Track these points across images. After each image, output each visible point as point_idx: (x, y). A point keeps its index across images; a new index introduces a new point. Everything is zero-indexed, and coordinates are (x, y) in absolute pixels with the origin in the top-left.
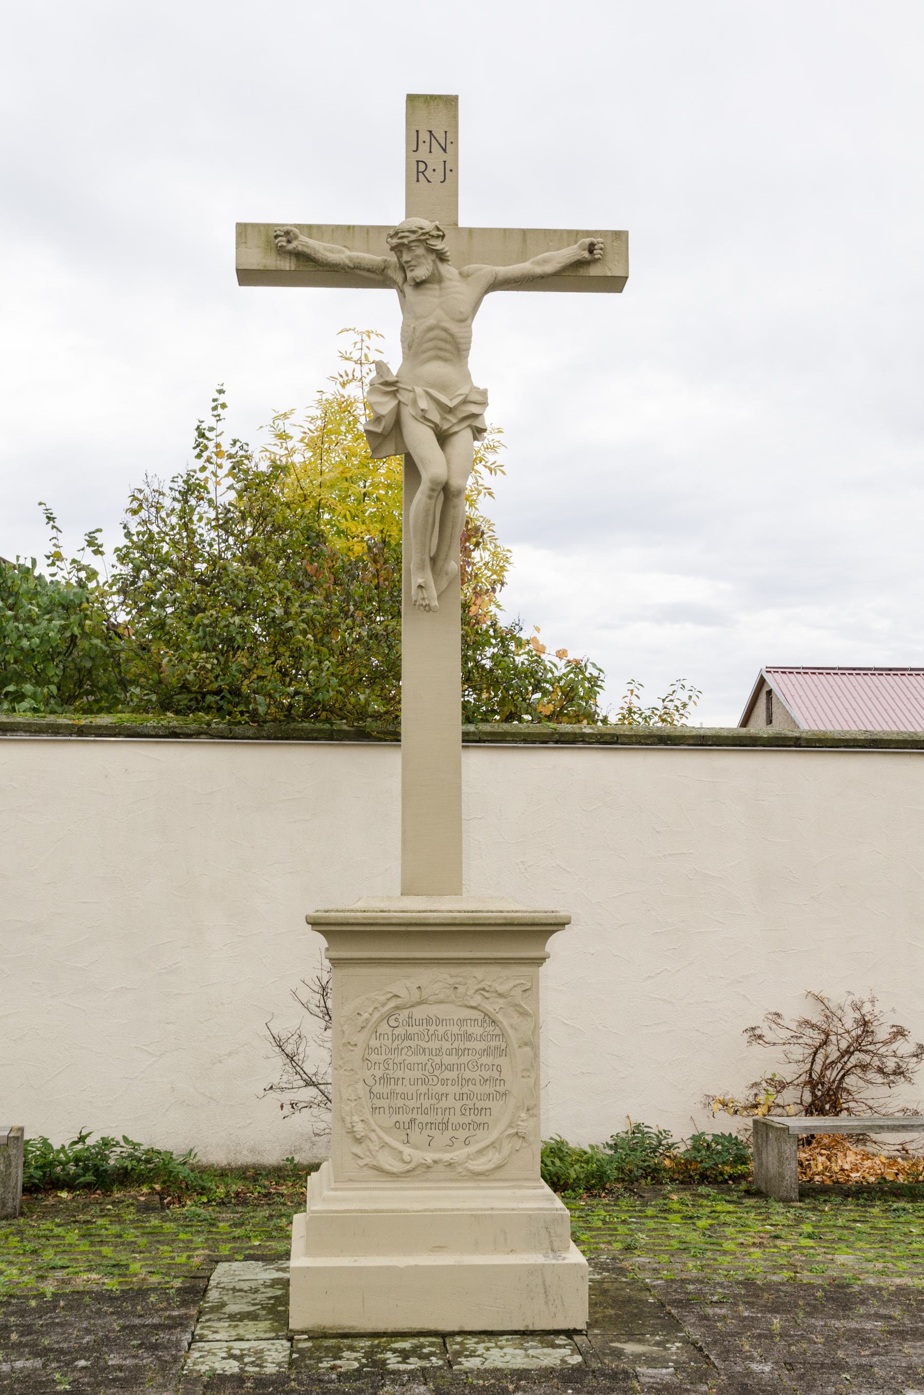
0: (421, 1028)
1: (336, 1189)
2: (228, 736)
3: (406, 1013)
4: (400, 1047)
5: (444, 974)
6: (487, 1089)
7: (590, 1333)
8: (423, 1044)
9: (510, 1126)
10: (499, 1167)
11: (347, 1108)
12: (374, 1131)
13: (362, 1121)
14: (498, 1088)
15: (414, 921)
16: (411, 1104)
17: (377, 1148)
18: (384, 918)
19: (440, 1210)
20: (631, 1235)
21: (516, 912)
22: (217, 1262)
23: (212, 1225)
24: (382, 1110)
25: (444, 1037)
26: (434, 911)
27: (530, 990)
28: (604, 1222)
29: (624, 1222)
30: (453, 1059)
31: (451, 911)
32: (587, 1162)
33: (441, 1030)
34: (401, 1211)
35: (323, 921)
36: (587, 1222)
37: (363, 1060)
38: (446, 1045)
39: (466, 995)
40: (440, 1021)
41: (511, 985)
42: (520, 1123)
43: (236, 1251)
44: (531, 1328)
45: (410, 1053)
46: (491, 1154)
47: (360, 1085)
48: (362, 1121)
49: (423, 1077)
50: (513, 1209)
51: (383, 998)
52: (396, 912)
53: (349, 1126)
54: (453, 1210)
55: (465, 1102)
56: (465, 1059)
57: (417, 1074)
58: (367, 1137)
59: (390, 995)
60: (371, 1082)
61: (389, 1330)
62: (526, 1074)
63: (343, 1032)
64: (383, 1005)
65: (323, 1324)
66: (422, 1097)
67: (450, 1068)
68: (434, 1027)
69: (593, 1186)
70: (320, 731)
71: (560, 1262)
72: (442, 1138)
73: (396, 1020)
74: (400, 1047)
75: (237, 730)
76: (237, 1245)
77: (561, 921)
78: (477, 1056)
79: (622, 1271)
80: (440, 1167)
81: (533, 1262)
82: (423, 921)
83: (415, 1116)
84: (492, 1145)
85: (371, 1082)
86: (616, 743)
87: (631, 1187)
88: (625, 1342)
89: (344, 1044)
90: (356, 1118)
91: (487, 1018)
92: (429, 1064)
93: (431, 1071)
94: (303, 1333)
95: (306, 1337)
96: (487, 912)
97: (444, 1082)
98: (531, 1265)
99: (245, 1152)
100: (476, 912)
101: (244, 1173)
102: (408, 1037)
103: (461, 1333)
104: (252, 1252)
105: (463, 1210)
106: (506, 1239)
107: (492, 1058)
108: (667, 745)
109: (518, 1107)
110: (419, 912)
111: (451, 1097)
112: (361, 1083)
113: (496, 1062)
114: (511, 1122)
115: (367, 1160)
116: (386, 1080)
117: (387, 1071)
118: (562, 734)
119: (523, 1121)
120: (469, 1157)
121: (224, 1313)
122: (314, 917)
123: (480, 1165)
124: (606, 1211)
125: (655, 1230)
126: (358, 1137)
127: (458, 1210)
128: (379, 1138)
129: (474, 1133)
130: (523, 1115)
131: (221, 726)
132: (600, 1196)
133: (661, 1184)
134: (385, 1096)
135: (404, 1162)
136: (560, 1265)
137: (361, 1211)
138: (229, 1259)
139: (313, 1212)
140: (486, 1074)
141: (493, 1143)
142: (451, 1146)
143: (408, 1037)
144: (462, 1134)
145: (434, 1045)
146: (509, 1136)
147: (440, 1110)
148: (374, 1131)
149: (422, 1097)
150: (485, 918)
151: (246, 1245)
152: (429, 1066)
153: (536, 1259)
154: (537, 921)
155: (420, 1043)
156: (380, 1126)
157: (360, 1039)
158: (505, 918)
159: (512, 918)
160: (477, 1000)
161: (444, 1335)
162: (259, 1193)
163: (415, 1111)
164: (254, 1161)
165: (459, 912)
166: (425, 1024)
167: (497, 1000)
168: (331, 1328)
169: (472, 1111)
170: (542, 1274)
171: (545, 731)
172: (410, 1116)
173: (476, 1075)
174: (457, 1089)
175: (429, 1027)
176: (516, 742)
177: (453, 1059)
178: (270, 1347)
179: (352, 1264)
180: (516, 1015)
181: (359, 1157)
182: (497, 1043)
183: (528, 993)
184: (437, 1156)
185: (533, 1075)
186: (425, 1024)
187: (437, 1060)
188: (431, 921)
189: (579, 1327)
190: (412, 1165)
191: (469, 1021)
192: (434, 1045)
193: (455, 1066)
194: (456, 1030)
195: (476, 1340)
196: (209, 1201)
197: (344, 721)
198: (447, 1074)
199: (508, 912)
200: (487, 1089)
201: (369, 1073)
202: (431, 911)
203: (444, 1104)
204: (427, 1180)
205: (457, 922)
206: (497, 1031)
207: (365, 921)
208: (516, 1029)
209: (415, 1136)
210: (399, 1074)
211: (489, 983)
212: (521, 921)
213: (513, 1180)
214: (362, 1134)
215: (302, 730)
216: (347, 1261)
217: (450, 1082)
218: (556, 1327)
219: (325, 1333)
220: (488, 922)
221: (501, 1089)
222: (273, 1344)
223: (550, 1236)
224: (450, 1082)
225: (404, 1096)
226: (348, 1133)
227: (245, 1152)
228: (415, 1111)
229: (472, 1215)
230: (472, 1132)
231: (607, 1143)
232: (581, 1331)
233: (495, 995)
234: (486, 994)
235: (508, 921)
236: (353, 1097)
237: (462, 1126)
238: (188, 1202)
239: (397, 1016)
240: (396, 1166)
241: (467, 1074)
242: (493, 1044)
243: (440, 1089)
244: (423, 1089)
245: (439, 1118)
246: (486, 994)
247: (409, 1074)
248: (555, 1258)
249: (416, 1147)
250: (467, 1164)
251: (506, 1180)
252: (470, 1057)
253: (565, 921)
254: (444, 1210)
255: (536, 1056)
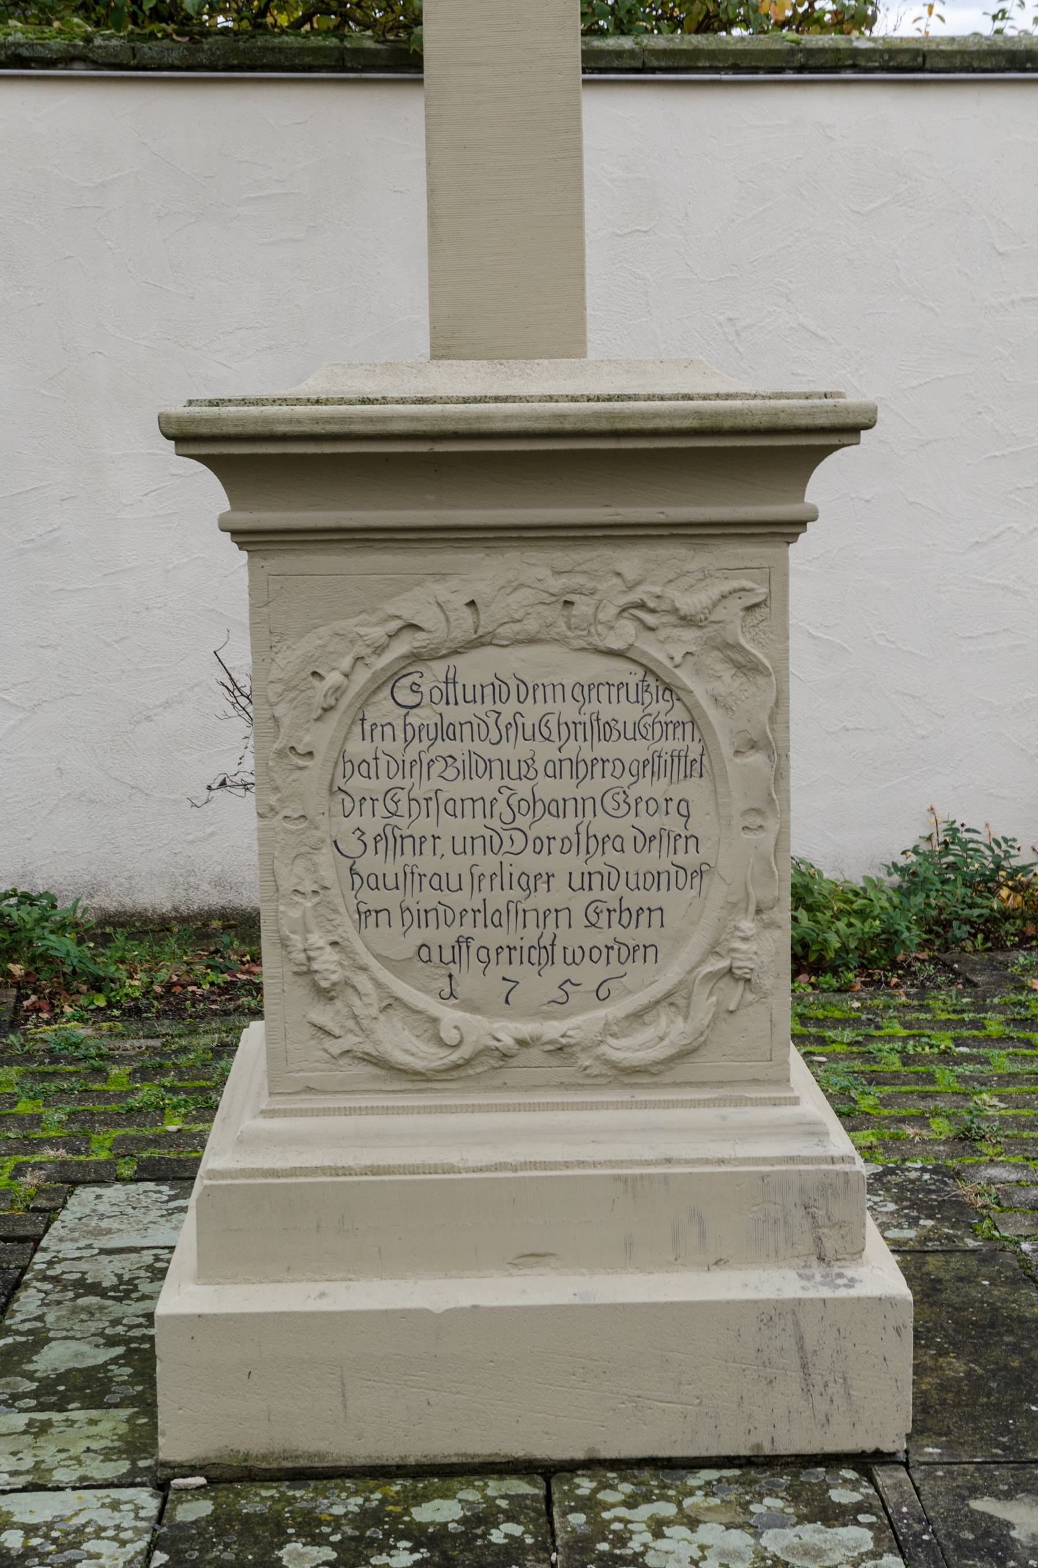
0: (479, 709)
1: (269, 1113)
2: (128, 66)
3: (439, 668)
4: (425, 759)
5: (538, 569)
6: (653, 860)
7: (914, 1458)
8: (485, 750)
9: (713, 951)
10: (684, 1054)
11: (295, 914)
12: (364, 969)
13: (334, 944)
14: (680, 858)
15: (451, 427)
16: (459, 900)
17: (374, 1011)
18: (371, 420)
19: (534, 1165)
20: (966, 1096)
21: (728, 396)
22: (76, 1183)
23: (99, 1073)
24: (383, 916)
25: (540, 731)
26: (505, 399)
27: (765, 607)
28: (907, 1059)
29: (945, 1056)
30: (563, 788)
31: (551, 398)
32: (863, 914)
33: (532, 712)
34: (434, 1169)
35: (204, 430)
36: (869, 1057)
37: (331, 793)
38: (545, 751)
39: (596, 621)
40: (527, 690)
41: (715, 592)
42: (738, 945)
43: (123, 1148)
44: (767, 1450)
45: (451, 773)
46: (663, 1020)
47: (326, 856)
48: (334, 944)
49: (487, 833)
50: (721, 1161)
51: (377, 633)
52: (402, 401)
53: (302, 957)
54: (567, 1165)
55: (596, 893)
56: (593, 787)
57: (472, 825)
58: (347, 983)
59: (394, 625)
60: (352, 847)
61: (412, 1461)
62: (755, 820)
63: (275, 719)
64: (379, 650)
65: (243, 1449)
66: (486, 883)
67: (555, 809)
68: (513, 705)
69: (873, 961)
70: (317, 51)
71: (842, 1293)
72: (538, 984)
73: (414, 688)
74: (425, 759)
75: (148, 50)
76: (132, 1131)
77: (850, 420)
78: (627, 779)
79: (959, 1212)
80: (535, 1054)
81: (773, 1296)
82: (476, 426)
83: (467, 930)
84: (667, 999)
85: (352, 847)
86: (921, 69)
87: (945, 956)
88: (1007, 1496)
89: (280, 754)
90: (317, 939)
91: (650, 680)
92: (502, 799)
93: (508, 817)
94: (192, 1470)
95: (201, 1481)
96: (650, 398)
97: (542, 845)
98: (766, 1302)
99: (205, 887)
100: (620, 398)
101: (205, 925)
102: (446, 731)
103: (592, 1465)
104: (156, 1153)
105: (595, 1164)
106: (703, 1235)
107: (664, 781)
108: (1024, 70)
109: (734, 905)
110: (466, 401)
111: (559, 883)
112: (328, 850)
113: (677, 792)
114: (717, 942)
115: (349, 1041)
116: (390, 840)
117: (395, 820)
118: (811, 52)
119: (745, 939)
120: (609, 1031)
121: (30, 1376)
122: (179, 420)
123: (634, 1048)
124: (907, 1025)
125: (1012, 1078)
126: (324, 984)
127: (581, 1164)
128: (378, 984)
129: (621, 970)
130: (747, 925)
131: (114, 42)
132: (888, 984)
133: (1003, 948)
134: (391, 883)
135: (441, 1043)
136: (843, 1301)
137: (335, 1171)
138: (102, 1177)
139: (213, 1174)
140: (650, 825)
141: (669, 995)
142: (561, 1002)
143: (446, 731)
144: (589, 974)
145: (513, 751)
146: (710, 977)
147: (531, 916)
148: (364, 969)
149: (486, 883)
150: (643, 415)
151: (148, 1132)
152: (501, 807)
153: (779, 1283)
154: (783, 421)
155: (478, 747)
156: (378, 957)
157: (320, 737)
158: (698, 414)
159: (716, 414)
160: (624, 634)
161: (549, 1471)
162: (212, 984)
163: (469, 918)
164: (222, 902)
165: (574, 399)
166: (489, 699)
167: (677, 632)
168: (264, 1458)
169: (615, 916)
170: (796, 1324)
171: (778, 47)
172: (456, 931)
173: (623, 826)
174: (575, 862)
175: (499, 707)
176: (717, 70)
177: (563, 788)
178: (105, 1518)
179: (311, 1306)
180: (727, 672)
181: (329, 1034)
182: (678, 745)
183: (759, 613)
184: (526, 1029)
185: (772, 825)
186: (489, 699)
187: (523, 788)
188: (498, 426)
189: (887, 1447)
190: (465, 1052)
191: (604, 690)
192: (513, 751)
193: (571, 804)
194: (569, 711)
195: (627, 1488)
196: (110, 1005)
197: (369, 33)
198: (549, 825)
199: (705, 397)
200: (653, 860)
201: (349, 824)
202: (497, 399)
203: (541, 899)
204: (505, 1087)
205: (568, 426)
206: (679, 714)
207: (318, 429)
208: (727, 708)
209: (470, 979)
210: (424, 826)
211: (657, 590)
212: (740, 422)
213: (720, 1084)
214: (334, 978)
215: (281, 50)
216: (321, 1247)
217: (555, 845)
218: (831, 1448)
219: (249, 1469)
220: (651, 425)
221: (690, 859)
222: (115, 1505)
223: (815, 1225)
224: (555, 845)
225: (440, 882)
226: (297, 974)
227: (205, 887)
228: (469, 918)
229: (617, 1178)
230: (615, 969)
231: (894, 865)
232: (893, 1454)
233: (672, 619)
234: (650, 619)
235: (707, 423)
236: (308, 886)
237: (590, 954)
238: (68, 1010)
239: (415, 678)
240: (424, 1055)
241: (602, 825)
242: (669, 746)
243: (531, 862)
244: (488, 863)
245: (531, 935)
246: (650, 619)
247: (449, 826)
248: (829, 1281)
249: (474, 1008)
250: (604, 1048)
251: (702, 1084)
252: (609, 782)
253: (861, 420)
254: (545, 1165)
255: (780, 775)
